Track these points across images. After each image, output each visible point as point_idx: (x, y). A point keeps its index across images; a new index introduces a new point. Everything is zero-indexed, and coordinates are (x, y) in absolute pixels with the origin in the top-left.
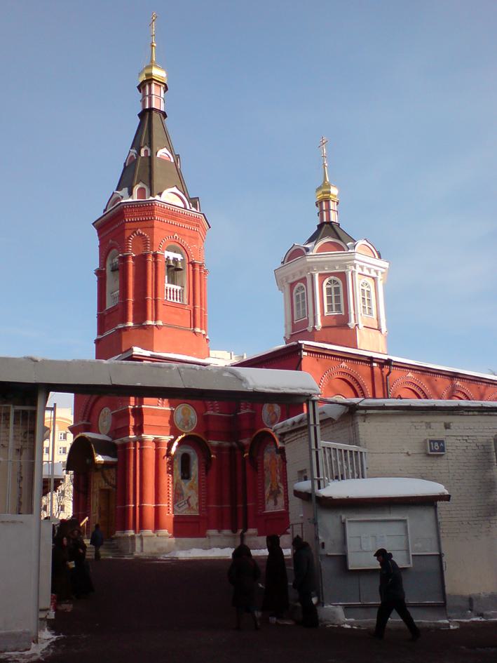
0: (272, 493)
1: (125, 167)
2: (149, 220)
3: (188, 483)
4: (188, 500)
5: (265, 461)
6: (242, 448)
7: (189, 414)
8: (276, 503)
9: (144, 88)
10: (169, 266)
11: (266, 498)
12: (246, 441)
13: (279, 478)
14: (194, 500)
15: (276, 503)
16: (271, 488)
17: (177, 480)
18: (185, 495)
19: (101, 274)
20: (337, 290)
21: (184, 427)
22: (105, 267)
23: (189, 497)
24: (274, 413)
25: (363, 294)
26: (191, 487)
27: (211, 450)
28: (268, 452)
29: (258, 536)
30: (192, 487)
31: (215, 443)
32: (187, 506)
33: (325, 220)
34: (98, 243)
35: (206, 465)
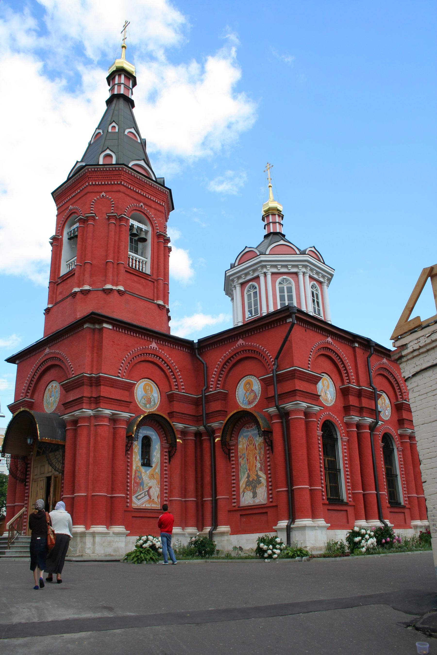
0: (248, 483)
1: (90, 144)
2: (114, 184)
3: (149, 471)
4: (148, 491)
5: (240, 446)
6: (211, 433)
7: (152, 391)
8: (255, 495)
9: (114, 79)
10: (133, 235)
11: (241, 490)
12: (215, 425)
13: (259, 465)
14: (155, 492)
15: (255, 495)
16: (248, 477)
17: (137, 466)
18: (145, 485)
19: (56, 242)
20: (290, 290)
21: (145, 405)
22: (62, 234)
23: (150, 488)
24: (252, 391)
25: (313, 296)
26: (152, 476)
27: (176, 433)
28: (245, 437)
29: (230, 534)
30: (153, 475)
31: (180, 426)
32: (147, 498)
33: (272, 231)
34: (56, 212)
35: (170, 450)
